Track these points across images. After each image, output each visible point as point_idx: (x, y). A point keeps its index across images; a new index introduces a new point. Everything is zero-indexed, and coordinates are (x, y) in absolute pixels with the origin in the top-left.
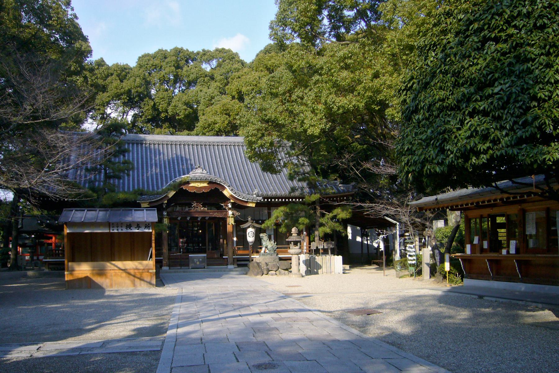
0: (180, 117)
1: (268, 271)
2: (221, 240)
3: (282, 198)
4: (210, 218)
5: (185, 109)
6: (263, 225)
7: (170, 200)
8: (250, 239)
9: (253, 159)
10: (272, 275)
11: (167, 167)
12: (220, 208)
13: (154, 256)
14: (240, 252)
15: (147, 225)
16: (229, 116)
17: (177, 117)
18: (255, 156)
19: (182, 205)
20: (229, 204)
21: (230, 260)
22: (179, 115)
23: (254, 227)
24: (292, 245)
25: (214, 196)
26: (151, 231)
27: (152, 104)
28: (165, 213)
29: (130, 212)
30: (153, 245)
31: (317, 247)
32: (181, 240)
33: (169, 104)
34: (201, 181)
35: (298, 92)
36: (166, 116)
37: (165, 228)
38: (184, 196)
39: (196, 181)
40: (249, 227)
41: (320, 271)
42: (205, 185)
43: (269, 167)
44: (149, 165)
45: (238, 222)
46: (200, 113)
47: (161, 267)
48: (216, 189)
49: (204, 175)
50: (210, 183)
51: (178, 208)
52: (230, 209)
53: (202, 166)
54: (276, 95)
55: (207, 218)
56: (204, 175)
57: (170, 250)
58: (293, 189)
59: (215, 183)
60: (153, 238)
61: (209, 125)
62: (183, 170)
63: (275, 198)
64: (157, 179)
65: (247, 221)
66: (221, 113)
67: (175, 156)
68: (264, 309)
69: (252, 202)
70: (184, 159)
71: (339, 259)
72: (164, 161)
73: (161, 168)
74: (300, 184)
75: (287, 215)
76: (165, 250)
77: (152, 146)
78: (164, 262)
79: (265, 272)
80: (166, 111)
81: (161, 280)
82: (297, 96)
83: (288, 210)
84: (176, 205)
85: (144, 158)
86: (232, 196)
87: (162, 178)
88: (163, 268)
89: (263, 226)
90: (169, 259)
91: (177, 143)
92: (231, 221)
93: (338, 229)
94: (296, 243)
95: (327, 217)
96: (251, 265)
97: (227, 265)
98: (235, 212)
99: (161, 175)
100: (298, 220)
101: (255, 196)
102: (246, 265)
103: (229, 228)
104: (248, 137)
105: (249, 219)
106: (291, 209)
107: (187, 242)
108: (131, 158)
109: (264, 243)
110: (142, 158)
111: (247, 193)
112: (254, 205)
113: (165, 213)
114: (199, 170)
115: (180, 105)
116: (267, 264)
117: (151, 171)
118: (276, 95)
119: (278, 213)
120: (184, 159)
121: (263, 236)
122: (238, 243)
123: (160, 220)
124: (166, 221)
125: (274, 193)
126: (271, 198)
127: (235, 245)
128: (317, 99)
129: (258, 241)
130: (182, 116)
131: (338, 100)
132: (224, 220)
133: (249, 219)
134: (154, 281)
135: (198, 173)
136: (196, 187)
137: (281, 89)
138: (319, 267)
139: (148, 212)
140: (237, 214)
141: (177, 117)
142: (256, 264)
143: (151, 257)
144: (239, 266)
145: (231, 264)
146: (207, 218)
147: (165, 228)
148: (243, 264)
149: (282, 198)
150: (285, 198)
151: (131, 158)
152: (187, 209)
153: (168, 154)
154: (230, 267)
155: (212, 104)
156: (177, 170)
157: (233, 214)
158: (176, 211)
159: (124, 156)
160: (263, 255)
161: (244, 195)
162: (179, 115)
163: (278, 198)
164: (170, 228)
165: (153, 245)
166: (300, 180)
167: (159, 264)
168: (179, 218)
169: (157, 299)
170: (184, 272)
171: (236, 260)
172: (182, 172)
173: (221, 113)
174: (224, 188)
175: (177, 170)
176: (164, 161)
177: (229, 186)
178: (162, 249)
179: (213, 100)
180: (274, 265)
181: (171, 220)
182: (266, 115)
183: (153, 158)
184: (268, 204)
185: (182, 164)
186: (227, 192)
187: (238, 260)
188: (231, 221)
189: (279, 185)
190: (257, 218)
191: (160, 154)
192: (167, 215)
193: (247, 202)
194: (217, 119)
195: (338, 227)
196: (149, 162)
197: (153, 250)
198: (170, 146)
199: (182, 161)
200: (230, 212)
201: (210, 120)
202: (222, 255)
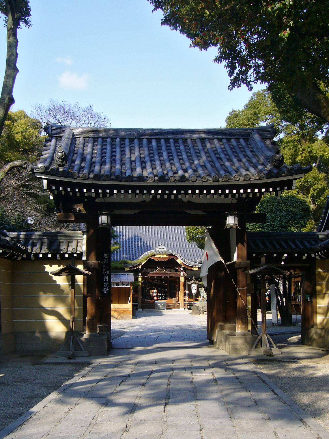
8: (194, 291)
15: (128, 284)
20: (181, 268)
23: (196, 283)
25: (171, 263)
26: (130, 287)
29: (118, 275)
34: (163, 254)
39: (160, 254)
40: (193, 283)
42: (165, 256)
47: (137, 309)
48: (173, 259)
49: (165, 250)
50: (169, 255)
52: (182, 271)
53: (163, 244)
55: (168, 277)
56: (165, 250)
59: (172, 255)
65: (192, 279)
76: (140, 297)
79: (202, 313)
85: (134, 251)
86: (182, 263)
92: (182, 280)
101: (197, 263)
108: (119, 241)
109: (202, 294)
111: (194, 260)
114: (162, 247)
116: (203, 307)
132: (178, 278)
135: (162, 248)
142: (196, 307)
143: (130, 302)
146: (168, 277)
151: (119, 241)
157: (184, 275)
159: (115, 239)
160: (201, 301)
161: (191, 262)
167: (135, 307)
170: (151, 312)
172: (149, 248)
174: (177, 258)
177: (180, 257)
181: (143, 278)
186: (179, 261)
188: (182, 280)
191: (123, 236)
193: (192, 267)
197: (131, 298)
199: (138, 239)
200: (182, 274)
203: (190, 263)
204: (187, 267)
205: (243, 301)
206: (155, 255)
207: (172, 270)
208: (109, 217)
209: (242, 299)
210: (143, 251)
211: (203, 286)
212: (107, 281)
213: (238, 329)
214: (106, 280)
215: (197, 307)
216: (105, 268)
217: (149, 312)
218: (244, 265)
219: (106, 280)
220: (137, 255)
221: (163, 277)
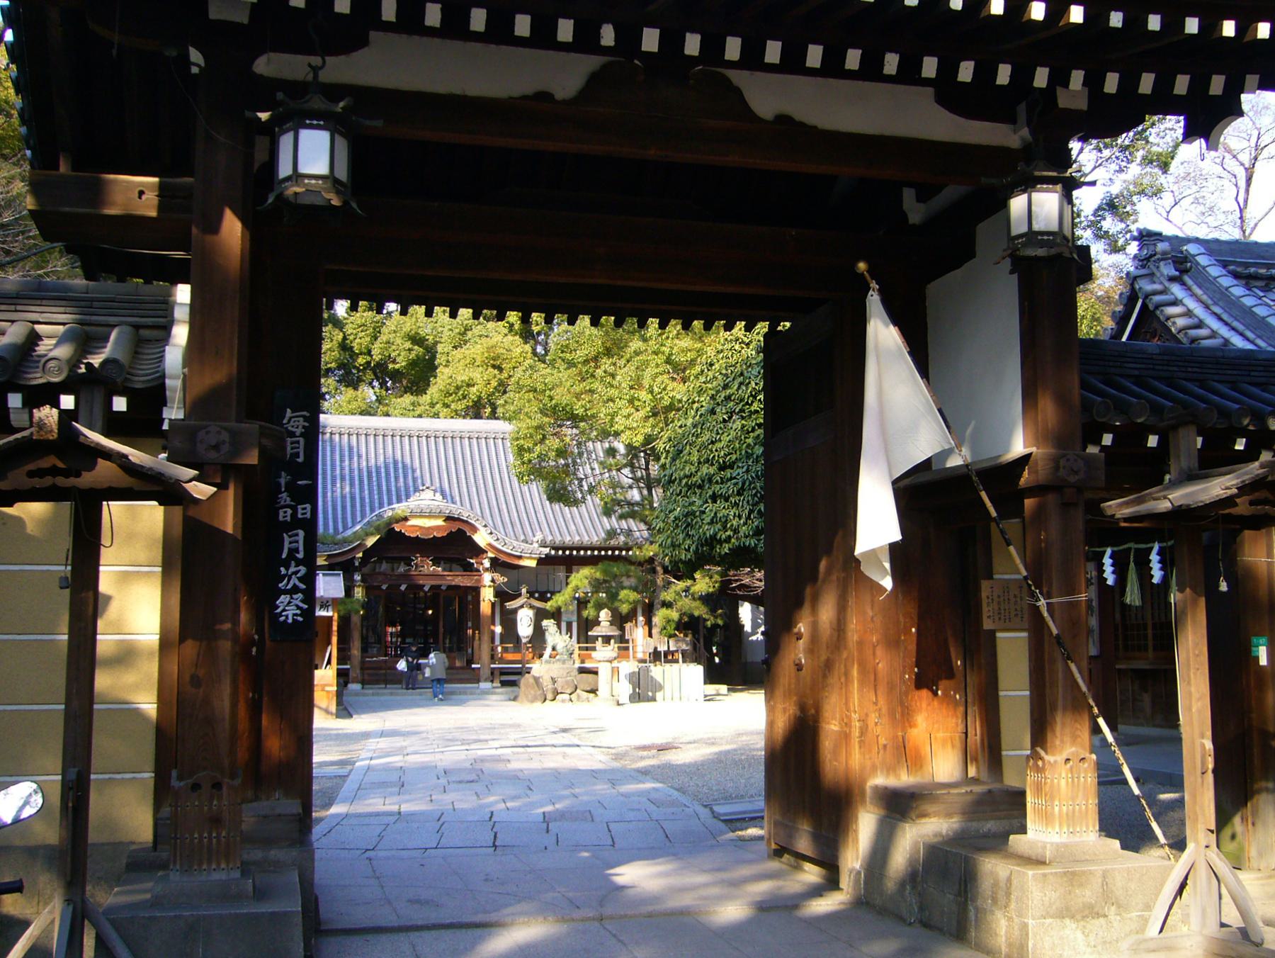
0: (397, 366)
1: (556, 693)
2: (470, 632)
3: (593, 549)
4: (450, 587)
5: (410, 350)
6: (549, 604)
7: (369, 553)
9: (526, 478)
10: (563, 701)
11: (366, 482)
12: (469, 568)
13: (334, 660)
14: (509, 656)
16: (500, 369)
17: (391, 366)
18: (535, 471)
19: (392, 560)
21: (485, 673)
22: (394, 362)
23: (531, 607)
24: (599, 643)
25: (456, 545)
26: (330, 614)
27: (340, 337)
28: (358, 577)
30: (335, 639)
31: (656, 648)
32: (390, 630)
33: (376, 339)
35: (606, 364)
36: (368, 363)
37: (357, 607)
38: (395, 544)
39: (421, 515)
40: (522, 607)
41: (659, 695)
42: (440, 522)
43: (559, 495)
44: (329, 477)
45: (503, 595)
46: (440, 359)
47: (346, 684)
48: (461, 532)
50: (449, 519)
51: (385, 566)
52: (487, 570)
54: (571, 364)
55: (444, 588)
57: (364, 650)
58: (612, 534)
60: (335, 628)
61: (458, 388)
62: (398, 490)
63: (578, 549)
64: (344, 508)
65: (520, 595)
66: (485, 364)
67: (381, 459)
68: (514, 743)
69: (531, 558)
70: (400, 465)
71: (697, 671)
72: (360, 470)
73: (352, 485)
74: (624, 524)
75: (597, 585)
76: (356, 652)
77: (337, 437)
78: (352, 674)
79: (550, 696)
80: (369, 353)
81: (346, 709)
82: (605, 372)
83: (598, 575)
84: (380, 561)
85: (339, 508)
86: (490, 545)
87: (353, 506)
88: (350, 686)
89: (549, 606)
90: (362, 669)
91: (387, 432)
92: (487, 595)
93: (696, 614)
94: (607, 640)
95: (673, 588)
96: (526, 680)
97: (478, 681)
98: (497, 576)
99: (353, 498)
100: (617, 594)
101: (536, 545)
102: (513, 684)
103: (485, 608)
104: (517, 439)
105: (524, 591)
106: (605, 572)
107: (402, 635)
110: (335, 509)
111: (522, 537)
112: (533, 564)
113: (358, 577)
114: (428, 494)
115: (399, 341)
116: (554, 681)
117: (333, 492)
118: (571, 364)
119: (581, 579)
120: (400, 465)
121: (548, 624)
122: (504, 639)
123: (349, 591)
124: (359, 593)
125: (577, 538)
126: (571, 549)
127: (497, 641)
128: (636, 384)
129: (539, 633)
130: (401, 363)
131: (671, 385)
132: (476, 591)
133: (524, 591)
134: (333, 708)
136: (421, 528)
137: (580, 354)
138: (658, 687)
139: (328, 578)
140: (501, 579)
141: (391, 366)
142: (531, 680)
143: (329, 662)
144: (504, 684)
145: (486, 680)
146: (444, 588)
147: (357, 607)
148: (510, 679)
149: (593, 549)
150: (600, 549)
152: (402, 569)
153: (373, 455)
154: (485, 685)
155: (466, 342)
156: (384, 488)
157: (493, 581)
158: (380, 573)
161: (515, 543)
162: (394, 362)
163: (586, 549)
164: (365, 606)
165: (335, 639)
166: (622, 517)
168: (384, 587)
169: (338, 735)
170: (391, 694)
171: (497, 673)
173: (485, 364)
174: (475, 529)
175: (384, 488)
176: (360, 470)
178: (349, 649)
179: (470, 333)
180: (567, 682)
181: (369, 589)
182: (551, 398)
183: (338, 463)
184: (564, 559)
185: (399, 479)
186: (481, 538)
187: (503, 672)
188: (487, 595)
189: (584, 525)
190: (542, 588)
192: (362, 581)
193: (520, 557)
194: (477, 375)
195: (697, 608)
196: (329, 472)
197: (333, 649)
198: (371, 439)
200: (487, 578)
201: (459, 378)
202: (470, 662)
203: (511, 546)
204: (503, 558)
205: (1073, 667)
206: (406, 519)
207: (454, 566)
208: (342, 144)
209: (1069, 658)
210: (368, 508)
211: (556, 615)
212: (301, 555)
213: (1047, 818)
214: (293, 552)
215: (536, 679)
216: (291, 488)
217: (383, 694)
218: (1076, 473)
219: (293, 552)
220: (349, 520)
221: (426, 589)
